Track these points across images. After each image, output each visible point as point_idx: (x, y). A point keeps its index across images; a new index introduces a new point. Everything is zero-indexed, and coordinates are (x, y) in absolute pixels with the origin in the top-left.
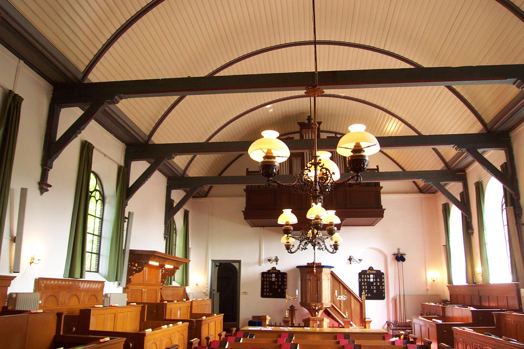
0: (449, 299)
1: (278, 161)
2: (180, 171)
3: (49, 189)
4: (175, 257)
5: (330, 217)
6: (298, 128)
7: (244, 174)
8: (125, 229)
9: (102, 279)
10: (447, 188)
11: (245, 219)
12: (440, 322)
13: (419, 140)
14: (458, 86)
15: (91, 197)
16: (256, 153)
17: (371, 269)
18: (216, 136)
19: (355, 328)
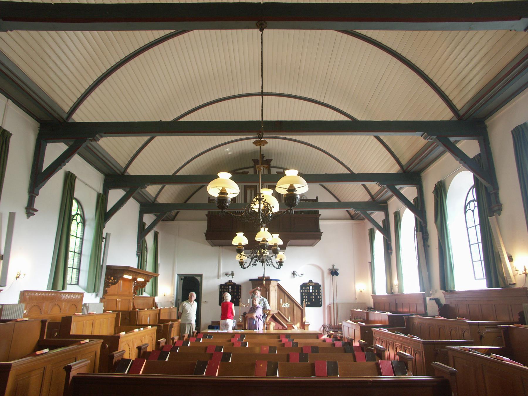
0: (372, 305)
1: (230, 196)
2: (150, 198)
3: (35, 213)
4: (146, 271)
5: (275, 239)
6: (252, 164)
7: (207, 202)
8: (103, 248)
9: (80, 290)
10: (372, 216)
11: (207, 239)
12: (364, 324)
13: (352, 177)
14: (383, 136)
15: (73, 220)
16: (213, 190)
17: (311, 281)
18: (183, 169)
19: (297, 329)
